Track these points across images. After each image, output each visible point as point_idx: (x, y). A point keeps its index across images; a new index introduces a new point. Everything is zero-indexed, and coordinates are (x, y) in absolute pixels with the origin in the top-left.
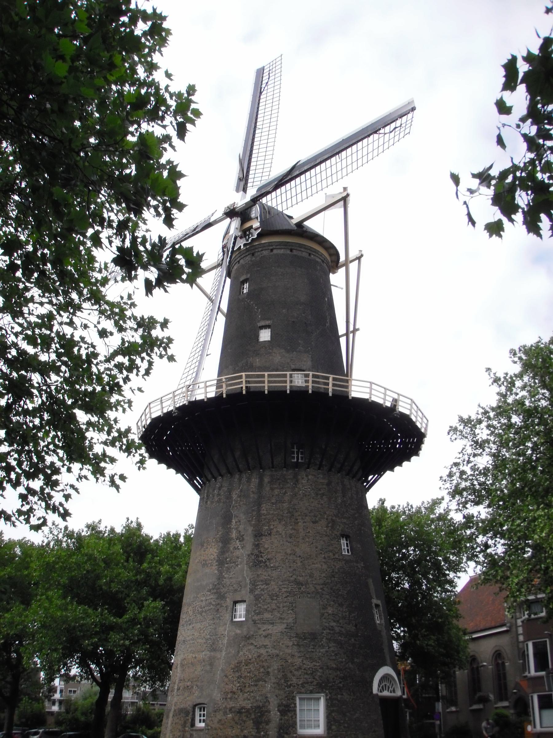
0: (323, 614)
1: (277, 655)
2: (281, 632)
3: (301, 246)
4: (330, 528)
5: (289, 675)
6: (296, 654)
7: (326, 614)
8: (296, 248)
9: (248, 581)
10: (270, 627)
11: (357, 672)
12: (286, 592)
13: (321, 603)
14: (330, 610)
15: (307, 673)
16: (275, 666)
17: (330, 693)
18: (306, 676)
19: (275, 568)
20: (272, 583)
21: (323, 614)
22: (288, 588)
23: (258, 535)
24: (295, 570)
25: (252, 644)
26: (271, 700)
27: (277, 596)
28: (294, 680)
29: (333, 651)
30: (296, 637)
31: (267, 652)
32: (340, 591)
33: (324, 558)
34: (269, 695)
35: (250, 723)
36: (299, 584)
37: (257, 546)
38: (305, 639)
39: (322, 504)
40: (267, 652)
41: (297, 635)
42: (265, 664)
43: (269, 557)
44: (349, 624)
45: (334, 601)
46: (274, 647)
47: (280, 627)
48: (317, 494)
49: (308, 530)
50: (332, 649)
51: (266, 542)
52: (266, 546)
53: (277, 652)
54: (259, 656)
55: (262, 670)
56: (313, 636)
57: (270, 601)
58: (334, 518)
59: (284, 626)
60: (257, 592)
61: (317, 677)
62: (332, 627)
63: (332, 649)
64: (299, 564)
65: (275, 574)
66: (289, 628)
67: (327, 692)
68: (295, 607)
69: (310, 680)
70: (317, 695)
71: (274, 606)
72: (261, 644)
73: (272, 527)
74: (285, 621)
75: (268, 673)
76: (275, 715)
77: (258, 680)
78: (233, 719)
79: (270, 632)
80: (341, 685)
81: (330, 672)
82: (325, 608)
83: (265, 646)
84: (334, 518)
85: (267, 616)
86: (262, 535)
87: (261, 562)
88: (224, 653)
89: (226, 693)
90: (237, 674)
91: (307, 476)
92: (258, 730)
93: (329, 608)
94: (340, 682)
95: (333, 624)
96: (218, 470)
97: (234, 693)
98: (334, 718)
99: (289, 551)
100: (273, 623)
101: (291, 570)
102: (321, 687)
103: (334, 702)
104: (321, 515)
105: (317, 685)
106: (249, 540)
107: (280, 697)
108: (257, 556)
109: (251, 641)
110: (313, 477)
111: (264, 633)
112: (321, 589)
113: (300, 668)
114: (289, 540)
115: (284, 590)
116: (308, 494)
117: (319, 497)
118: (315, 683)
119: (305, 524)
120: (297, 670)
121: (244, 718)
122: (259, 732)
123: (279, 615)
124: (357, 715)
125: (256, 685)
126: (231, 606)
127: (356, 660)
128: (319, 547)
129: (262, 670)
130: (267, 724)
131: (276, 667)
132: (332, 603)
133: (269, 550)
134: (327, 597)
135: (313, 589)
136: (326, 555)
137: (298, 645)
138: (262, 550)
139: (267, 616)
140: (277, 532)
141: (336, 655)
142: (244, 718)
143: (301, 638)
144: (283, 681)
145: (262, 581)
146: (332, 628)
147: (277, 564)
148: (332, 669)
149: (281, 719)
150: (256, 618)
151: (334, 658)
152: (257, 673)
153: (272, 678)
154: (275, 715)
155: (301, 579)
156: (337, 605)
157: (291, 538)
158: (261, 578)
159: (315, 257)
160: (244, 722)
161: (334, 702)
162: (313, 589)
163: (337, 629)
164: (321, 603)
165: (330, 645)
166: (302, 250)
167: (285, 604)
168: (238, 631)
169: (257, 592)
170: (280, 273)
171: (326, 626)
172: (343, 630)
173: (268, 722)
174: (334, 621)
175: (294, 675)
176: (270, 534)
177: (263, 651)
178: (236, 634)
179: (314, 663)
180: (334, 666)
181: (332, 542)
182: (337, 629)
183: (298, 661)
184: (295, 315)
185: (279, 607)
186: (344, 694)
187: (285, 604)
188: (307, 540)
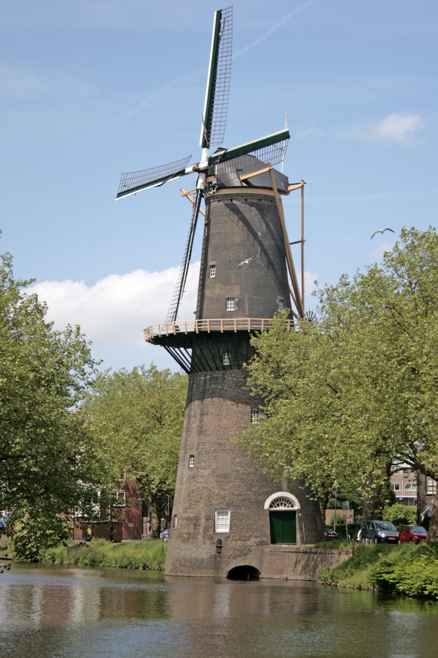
0: (233, 463)
1: (206, 488)
2: (209, 474)
3: (252, 195)
4: (243, 408)
5: (211, 499)
6: (216, 487)
7: (235, 463)
8: (234, 198)
9: (196, 443)
10: (204, 471)
11: (253, 497)
12: (213, 450)
13: (233, 456)
14: (238, 460)
15: (221, 498)
16: (205, 493)
17: (233, 509)
18: (220, 499)
19: (209, 435)
20: (207, 444)
21: (233, 463)
22: (214, 447)
23: (202, 414)
24: (219, 436)
25: (195, 481)
26: (202, 513)
27: (209, 452)
28: (214, 502)
29: (237, 485)
30: (216, 477)
31: (202, 486)
32: (65, 463)
33: (237, 428)
34: (201, 510)
35: (192, 526)
36: (220, 445)
37: (201, 421)
38: (221, 478)
39: (239, 392)
40: (202, 486)
41: (217, 476)
42: (200, 493)
43: (206, 428)
44: (251, 468)
45: (241, 454)
46: (205, 483)
47: (209, 471)
48: (236, 386)
49: (229, 410)
50: (237, 483)
51: (205, 418)
52: (205, 422)
53: (207, 485)
54: (198, 488)
55: (199, 496)
56: (226, 476)
57: (205, 455)
58: (247, 401)
59: (210, 470)
60: (199, 450)
61: (226, 500)
62: (238, 470)
63: (237, 483)
64: (222, 432)
65: (208, 439)
66: (213, 472)
67: (232, 508)
68: (217, 459)
69: (222, 502)
70: (226, 510)
71: (206, 459)
72: (199, 481)
73: (209, 409)
74: (211, 468)
75: (201, 498)
76: (203, 521)
77: (196, 502)
78: (185, 523)
79: (203, 474)
80: (241, 504)
81: (235, 497)
82: (234, 459)
83: (201, 482)
84: (247, 401)
85: (203, 464)
86: (204, 414)
87: (202, 431)
88: (184, 486)
89: (184, 509)
90: (188, 499)
91: (231, 374)
92: (195, 529)
93: (237, 459)
94: (240, 503)
95: (239, 468)
96: (199, 368)
97: (187, 509)
98: (234, 523)
99: (216, 425)
100: (205, 469)
101: (217, 436)
102: (229, 505)
103: (235, 514)
104: (238, 399)
105: (226, 504)
106: (198, 416)
107: (207, 511)
108: (201, 428)
109: (195, 479)
110: (235, 375)
111: (201, 475)
112: (234, 447)
113: (217, 495)
114: (217, 417)
115: (212, 449)
116: (230, 386)
117: (238, 387)
118: (225, 503)
119: (227, 407)
120: (215, 496)
121: (190, 523)
122: (195, 531)
123: (208, 464)
124: (250, 521)
125: (196, 505)
126: (188, 458)
127: (253, 489)
128: (235, 421)
129: (199, 496)
130: (199, 526)
131: (205, 494)
132: (240, 455)
133: (207, 424)
134: (237, 452)
135: (229, 448)
136: (239, 426)
137: (217, 481)
138: (203, 424)
139: (203, 464)
140: (211, 412)
141: (239, 486)
142: (190, 523)
143: (219, 477)
144: (208, 502)
145: (202, 443)
146: (238, 471)
147: (210, 433)
148: (236, 495)
149: (206, 524)
150: (198, 465)
151: (237, 488)
152: (196, 498)
153: (203, 500)
154: (203, 521)
155: (222, 441)
156: (243, 456)
157: (218, 416)
158: (202, 442)
159: (251, 200)
160: (190, 525)
161: (235, 514)
162: (229, 448)
163: (242, 471)
164: (233, 456)
165: (236, 481)
166: (239, 198)
167: (212, 457)
168: (190, 473)
169: (199, 450)
170: (223, 221)
171: (234, 470)
172: (246, 471)
173: (199, 525)
174: (240, 467)
175: (214, 499)
176: (207, 414)
177: (200, 485)
178: (190, 475)
179: (225, 492)
180: (238, 493)
181: (244, 417)
182: (242, 471)
183: (216, 491)
184: (231, 255)
185: (209, 459)
186: (242, 509)
187: (212, 457)
188: (228, 417)
